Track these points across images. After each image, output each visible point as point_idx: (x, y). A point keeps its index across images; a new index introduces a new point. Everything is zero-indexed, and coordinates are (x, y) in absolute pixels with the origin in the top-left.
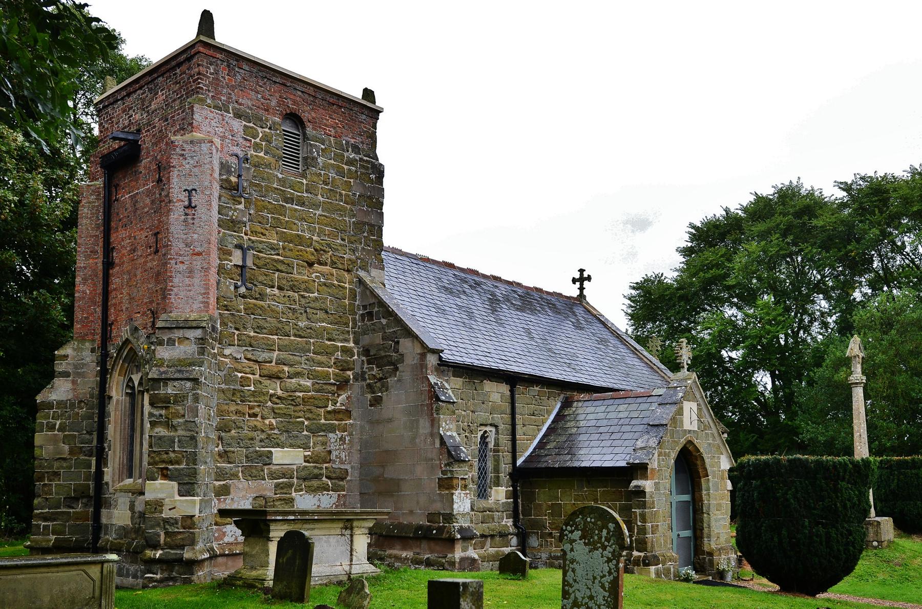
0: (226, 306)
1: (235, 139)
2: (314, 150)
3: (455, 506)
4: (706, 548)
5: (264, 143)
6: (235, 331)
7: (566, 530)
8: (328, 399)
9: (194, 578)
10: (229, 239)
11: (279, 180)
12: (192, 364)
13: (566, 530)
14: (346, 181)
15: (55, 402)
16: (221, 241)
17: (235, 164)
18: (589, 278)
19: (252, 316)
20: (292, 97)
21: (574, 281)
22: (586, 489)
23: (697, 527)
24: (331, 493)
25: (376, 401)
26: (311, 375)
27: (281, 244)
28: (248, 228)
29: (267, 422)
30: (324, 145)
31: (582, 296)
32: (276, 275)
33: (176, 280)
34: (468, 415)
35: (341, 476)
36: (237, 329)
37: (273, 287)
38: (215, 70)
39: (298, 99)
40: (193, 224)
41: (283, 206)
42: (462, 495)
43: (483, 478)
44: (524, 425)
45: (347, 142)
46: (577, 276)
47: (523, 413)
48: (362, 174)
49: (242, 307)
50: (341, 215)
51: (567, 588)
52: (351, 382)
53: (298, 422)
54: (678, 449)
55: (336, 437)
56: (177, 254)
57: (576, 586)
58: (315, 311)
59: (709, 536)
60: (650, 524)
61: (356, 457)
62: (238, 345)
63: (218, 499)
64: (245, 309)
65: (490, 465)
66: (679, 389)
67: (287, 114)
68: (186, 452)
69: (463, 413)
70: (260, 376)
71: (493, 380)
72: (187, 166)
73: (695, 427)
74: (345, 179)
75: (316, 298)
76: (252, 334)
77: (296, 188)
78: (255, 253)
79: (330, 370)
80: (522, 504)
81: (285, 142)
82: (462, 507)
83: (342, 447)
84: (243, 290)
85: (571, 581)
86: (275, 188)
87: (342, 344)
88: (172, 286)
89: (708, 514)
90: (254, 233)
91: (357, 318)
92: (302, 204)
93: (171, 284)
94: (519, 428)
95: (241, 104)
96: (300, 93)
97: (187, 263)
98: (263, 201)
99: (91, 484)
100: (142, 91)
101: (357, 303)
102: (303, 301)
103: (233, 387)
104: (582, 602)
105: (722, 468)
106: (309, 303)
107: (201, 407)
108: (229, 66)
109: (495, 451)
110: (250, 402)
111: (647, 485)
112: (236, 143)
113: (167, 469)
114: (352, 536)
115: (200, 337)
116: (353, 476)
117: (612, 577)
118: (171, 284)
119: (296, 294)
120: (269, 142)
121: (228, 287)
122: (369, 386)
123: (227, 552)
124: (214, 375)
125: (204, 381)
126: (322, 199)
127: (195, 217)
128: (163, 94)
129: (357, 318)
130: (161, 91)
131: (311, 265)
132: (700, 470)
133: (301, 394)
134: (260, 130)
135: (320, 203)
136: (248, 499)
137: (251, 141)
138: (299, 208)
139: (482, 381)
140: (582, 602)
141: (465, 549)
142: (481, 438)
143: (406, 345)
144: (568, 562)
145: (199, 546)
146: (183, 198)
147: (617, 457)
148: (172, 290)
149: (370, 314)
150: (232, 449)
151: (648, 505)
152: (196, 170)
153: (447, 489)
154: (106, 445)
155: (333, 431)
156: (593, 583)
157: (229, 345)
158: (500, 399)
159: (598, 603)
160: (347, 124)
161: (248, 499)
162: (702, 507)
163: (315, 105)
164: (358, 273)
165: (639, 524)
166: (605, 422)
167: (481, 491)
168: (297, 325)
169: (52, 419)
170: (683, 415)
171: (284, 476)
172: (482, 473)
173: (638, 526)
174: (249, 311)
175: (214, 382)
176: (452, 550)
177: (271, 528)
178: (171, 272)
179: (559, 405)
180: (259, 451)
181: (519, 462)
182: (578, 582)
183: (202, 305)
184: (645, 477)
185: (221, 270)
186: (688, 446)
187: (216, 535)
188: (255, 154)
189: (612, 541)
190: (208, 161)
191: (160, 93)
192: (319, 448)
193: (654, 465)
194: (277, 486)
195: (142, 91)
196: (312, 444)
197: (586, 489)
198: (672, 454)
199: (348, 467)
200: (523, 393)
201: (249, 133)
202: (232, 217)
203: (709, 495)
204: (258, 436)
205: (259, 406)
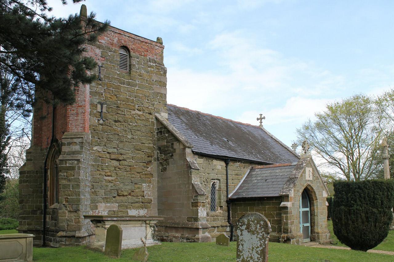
0: (94, 129)
1: (97, 57)
3: (199, 214)
4: (316, 231)
9: (81, 244)
11: (118, 74)
13: (239, 225)
15: (26, 172)
18: (264, 118)
19: (106, 133)
21: (258, 119)
22: (260, 206)
23: (312, 222)
25: (164, 170)
27: (119, 102)
30: (139, 59)
31: (261, 125)
33: (71, 118)
35: (149, 201)
36: (99, 139)
39: (127, 40)
40: (78, 93)
41: (119, 85)
42: (203, 209)
43: (214, 202)
44: (232, 179)
46: (259, 117)
47: (232, 174)
50: (147, 90)
51: (239, 253)
52: (153, 161)
54: (303, 188)
57: (244, 252)
58: (135, 131)
59: (317, 226)
60: (290, 221)
61: (156, 194)
63: (92, 211)
65: (217, 197)
67: (121, 46)
68: (75, 191)
69: (204, 174)
71: (217, 160)
73: (311, 179)
75: (136, 125)
77: (126, 78)
80: (232, 213)
84: (101, 122)
85: (241, 250)
86: (116, 78)
88: (69, 120)
91: (155, 134)
93: (69, 120)
95: (100, 42)
96: (127, 37)
97: (76, 110)
98: (110, 83)
99: (43, 205)
101: (155, 128)
102: (129, 126)
103: (97, 164)
106: (132, 127)
107: (82, 172)
109: (219, 191)
110: (106, 170)
111: (288, 204)
112: (98, 59)
113: (67, 198)
116: (155, 202)
117: (262, 248)
118: (69, 120)
121: (94, 121)
122: (161, 163)
124: (89, 158)
125: (83, 161)
126: (138, 83)
129: (155, 134)
132: (314, 197)
135: (137, 84)
136: (106, 211)
139: (212, 160)
141: (204, 233)
142: (212, 185)
143: (176, 145)
145: (83, 230)
147: (276, 192)
148: (69, 122)
149: (161, 132)
151: (289, 213)
153: (196, 207)
156: (252, 250)
158: (221, 168)
161: (106, 211)
162: (314, 213)
163: (134, 43)
164: (155, 114)
165: (285, 221)
166: (270, 178)
167: (213, 208)
168: (127, 137)
169: (26, 178)
170: (305, 173)
172: (213, 200)
173: (284, 222)
175: (89, 161)
176: (198, 233)
177: (106, 223)
178: (68, 114)
179: (249, 171)
181: (229, 196)
183: (82, 128)
184: (288, 201)
186: (308, 187)
193: (292, 194)
197: (260, 206)
198: (300, 190)
199: (152, 198)
200: (232, 166)
202: (96, 90)
203: (317, 208)
204: (110, 185)
205: (110, 172)
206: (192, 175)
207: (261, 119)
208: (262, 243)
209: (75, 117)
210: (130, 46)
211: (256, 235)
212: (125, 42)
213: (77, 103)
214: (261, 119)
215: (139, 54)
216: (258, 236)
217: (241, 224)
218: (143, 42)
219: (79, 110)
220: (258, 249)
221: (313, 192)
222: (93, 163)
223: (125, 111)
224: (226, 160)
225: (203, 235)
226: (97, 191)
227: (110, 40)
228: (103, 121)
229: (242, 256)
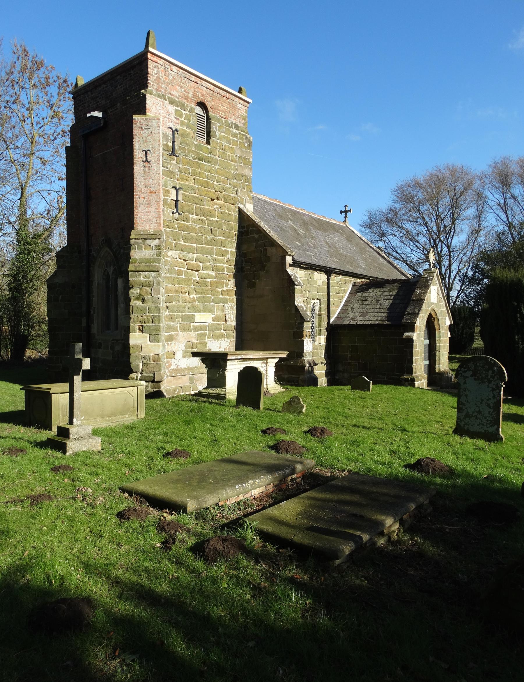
0: (168, 225)
2: (214, 127)
5: (186, 121)
6: (173, 241)
7: (461, 370)
8: (224, 283)
10: (169, 182)
12: (154, 262)
14: (231, 147)
16: (165, 185)
17: (170, 134)
20: (201, 91)
21: (341, 212)
24: (226, 339)
26: (215, 269)
28: (178, 176)
29: (191, 296)
32: (195, 206)
34: (306, 293)
36: (174, 240)
37: (193, 214)
38: (157, 71)
39: (204, 93)
40: (149, 173)
45: (232, 122)
46: (343, 210)
48: (240, 142)
49: (176, 226)
50: (229, 170)
53: (208, 297)
55: (228, 306)
56: (140, 192)
62: (175, 250)
64: (179, 228)
66: (428, 278)
70: (187, 269)
72: (144, 135)
74: (231, 146)
76: (182, 243)
78: (183, 192)
79: (225, 265)
81: (198, 122)
82: (308, 348)
83: (232, 312)
84: (176, 215)
85: (464, 402)
86: (193, 151)
87: (231, 250)
89: (439, 351)
90: (182, 179)
92: (209, 162)
94: (331, 300)
95: (172, 95)
96: (205, 88)
97: (146, 198)
100: (105, 86)
104: (472, 415)
105: (446, 325)
108: (165, 69)
114: (266, 367)
115: (158, 245)
117: (495, 400)
119: (205, 218)
120: (189, 120)
121: (169, 213)
123: (173, 375)
126: (218, 158)
127: (150, 168)
128: (121, 87)
130: (120, 85)
131: (213, 200)
133: (209, 280)
134: (184, 112)
137: (178, 119)
138: (206, 164)
140: (472, 415)
144: (461, 390)
146: (142, 156)
150: (174, 314)
152: (149, 137)
154: (92, 310)
155: (227, 303)
156: (481, 403)
157: (171, 250)
159: (485, 416)
160: (231, 110)
171: (202, 330)
174: (181, 229)
180: (189, 315)
182: (469, 403)
185: (165, 203)
187: (167, 365)
188: (181, 128)
189: (496, 378)
190: (157, 132)
191: (119, 87)
192: (219, 313)
194: (198, 335)
195: (105, 86)
196: (215, 310)
201: (178, 114)
206: (296, 294)
207: (346, 212)
208: (496, 394)
209: (147, 209)
210: (209, 103)
211: (487, 383)
212: (203, 95)
213: (149, 188)
214: (346, 212)
215: (219, 115)
216: (490, 385)
217: (464, 370)
218: (224, 97)
219: (151, 198)
220: (489, 402)
221: (436, 319)
222: (168, 275)
223: (204, 200)
224: (329, 272)
225: (308, 375)
226: (173, 315)
227: (184, 92)
228: (179, 214)
229: (466, 410)
